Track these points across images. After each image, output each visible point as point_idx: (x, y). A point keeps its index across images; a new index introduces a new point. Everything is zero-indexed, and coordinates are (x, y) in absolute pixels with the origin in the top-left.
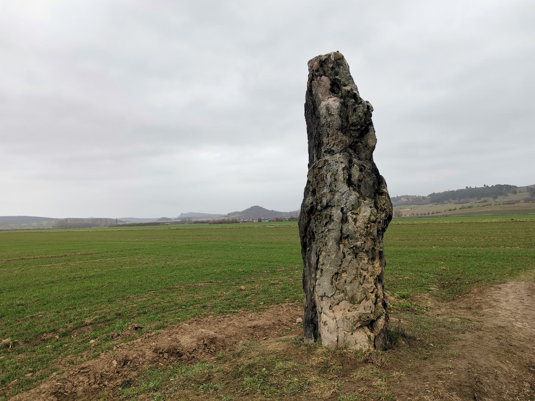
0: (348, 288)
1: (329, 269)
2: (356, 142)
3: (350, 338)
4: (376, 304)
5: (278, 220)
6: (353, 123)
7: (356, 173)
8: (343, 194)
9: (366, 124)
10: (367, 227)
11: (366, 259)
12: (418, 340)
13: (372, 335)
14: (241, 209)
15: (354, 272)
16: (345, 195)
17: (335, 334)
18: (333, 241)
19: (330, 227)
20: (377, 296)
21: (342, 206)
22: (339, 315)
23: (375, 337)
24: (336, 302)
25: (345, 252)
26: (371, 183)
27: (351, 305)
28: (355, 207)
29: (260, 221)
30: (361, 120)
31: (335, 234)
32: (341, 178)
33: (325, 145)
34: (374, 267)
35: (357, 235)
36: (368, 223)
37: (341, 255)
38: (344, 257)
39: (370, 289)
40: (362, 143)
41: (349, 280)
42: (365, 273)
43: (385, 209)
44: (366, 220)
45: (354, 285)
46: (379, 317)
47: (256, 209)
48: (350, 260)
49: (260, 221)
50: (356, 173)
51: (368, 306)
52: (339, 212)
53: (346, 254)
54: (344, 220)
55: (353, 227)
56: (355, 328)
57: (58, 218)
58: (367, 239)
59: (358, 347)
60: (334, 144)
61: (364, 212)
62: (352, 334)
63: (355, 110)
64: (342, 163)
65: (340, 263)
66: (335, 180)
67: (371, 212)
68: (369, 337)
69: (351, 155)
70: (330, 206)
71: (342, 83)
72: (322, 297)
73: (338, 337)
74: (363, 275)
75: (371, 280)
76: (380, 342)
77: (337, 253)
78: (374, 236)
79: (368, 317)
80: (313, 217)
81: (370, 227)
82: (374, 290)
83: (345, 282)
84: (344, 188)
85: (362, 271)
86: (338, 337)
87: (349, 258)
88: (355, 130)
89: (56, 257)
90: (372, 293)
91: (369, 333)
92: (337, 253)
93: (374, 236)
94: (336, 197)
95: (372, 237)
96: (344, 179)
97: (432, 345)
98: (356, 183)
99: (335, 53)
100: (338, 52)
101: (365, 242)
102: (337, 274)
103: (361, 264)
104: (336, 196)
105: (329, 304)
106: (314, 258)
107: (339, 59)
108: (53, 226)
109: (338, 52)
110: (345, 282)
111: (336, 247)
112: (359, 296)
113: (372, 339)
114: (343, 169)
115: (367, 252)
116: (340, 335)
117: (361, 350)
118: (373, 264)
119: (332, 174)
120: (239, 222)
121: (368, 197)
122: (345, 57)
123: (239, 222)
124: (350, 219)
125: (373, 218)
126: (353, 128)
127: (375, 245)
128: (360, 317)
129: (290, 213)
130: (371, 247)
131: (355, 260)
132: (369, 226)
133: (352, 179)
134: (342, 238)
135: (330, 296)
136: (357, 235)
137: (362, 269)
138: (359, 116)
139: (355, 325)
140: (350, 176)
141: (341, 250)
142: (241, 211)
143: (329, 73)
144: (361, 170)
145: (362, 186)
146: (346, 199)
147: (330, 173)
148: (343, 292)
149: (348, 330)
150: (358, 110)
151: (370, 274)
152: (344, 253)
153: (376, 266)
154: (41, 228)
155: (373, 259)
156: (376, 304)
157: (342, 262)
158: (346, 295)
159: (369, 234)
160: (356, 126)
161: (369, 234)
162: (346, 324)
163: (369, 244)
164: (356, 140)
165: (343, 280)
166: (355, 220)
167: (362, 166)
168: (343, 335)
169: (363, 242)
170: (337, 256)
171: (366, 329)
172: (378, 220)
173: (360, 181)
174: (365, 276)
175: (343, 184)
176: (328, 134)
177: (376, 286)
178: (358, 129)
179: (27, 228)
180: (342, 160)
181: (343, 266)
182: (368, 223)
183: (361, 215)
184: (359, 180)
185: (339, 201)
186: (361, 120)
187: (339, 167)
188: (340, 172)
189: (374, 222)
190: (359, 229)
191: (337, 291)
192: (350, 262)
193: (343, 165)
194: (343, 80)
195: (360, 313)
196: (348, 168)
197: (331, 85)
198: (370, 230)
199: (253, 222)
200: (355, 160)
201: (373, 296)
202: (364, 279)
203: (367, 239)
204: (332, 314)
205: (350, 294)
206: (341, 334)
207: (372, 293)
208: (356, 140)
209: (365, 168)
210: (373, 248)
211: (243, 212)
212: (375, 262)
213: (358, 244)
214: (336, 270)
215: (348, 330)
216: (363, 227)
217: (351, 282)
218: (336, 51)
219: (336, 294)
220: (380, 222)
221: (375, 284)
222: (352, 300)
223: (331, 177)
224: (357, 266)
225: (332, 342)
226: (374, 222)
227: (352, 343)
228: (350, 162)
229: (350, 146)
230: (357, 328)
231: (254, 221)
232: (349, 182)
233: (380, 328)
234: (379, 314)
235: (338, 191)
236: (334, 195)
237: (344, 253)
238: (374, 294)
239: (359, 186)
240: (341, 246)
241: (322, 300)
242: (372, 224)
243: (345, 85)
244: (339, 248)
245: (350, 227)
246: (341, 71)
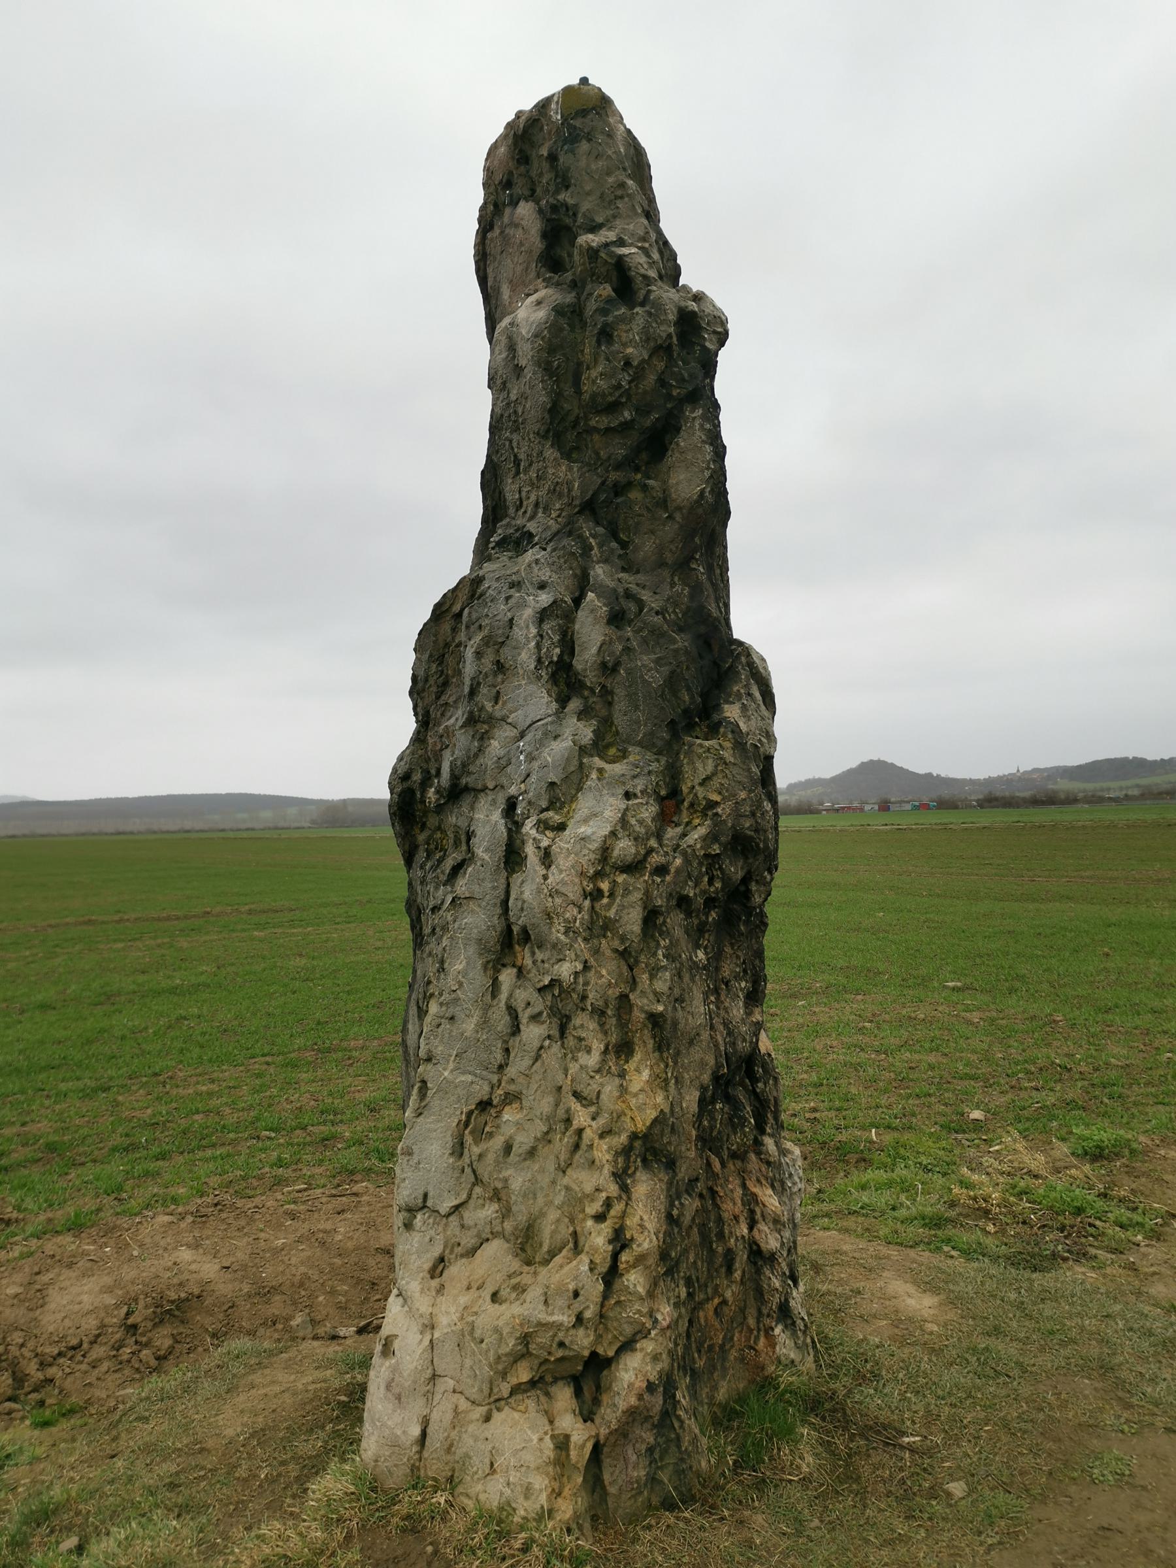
0: (518, 1182)
1: (454, 1081)
2: (619, 490)
3: (476, 1441)
4: (611, 1275)
5: (945, 805)
6: (594, 396)
7: (591, 632)
8: (522, 735)
9: (669, 397)
10: (596, 895)
11: (597, 1046)
12: (912, 1449)
13: (580, 1435)
14: (829, 771)
15: (545, 1105)
16: (528, 738)
17: (417, 1407)
18: (472, 950)
19: (462, 885)
20: (620, 1241)
21: (513, 790)
22: (448, 1315)
23: (597, 1449)
24: (468, 1240)
25: (519, 1005)
26: (656, 678)
27: (516, 1265)
28: (560, 796)
29: (885, 806)
30: (636, 378)
31: (477, 921)
32: (526, 658)
33: (511, 511)
34: (623, 1090)
35: (557, 933)
36: (599, 875)
37: (501, 1021)
38: (516, 1030)
39: (591, 1198)
40: (645, 488)
41: (523, 1141)
42: (581, 1117)
43: (713, 805)
44: (588, 858)
45: (542, 1170)
46: (627, 1346)
47: (875, 770)
48: (536, 1044)
49: (885, 806)
50: (591, 632)
51: (560, 1291)
52: (497, 816)
53: (524, 1018)
54: (512, 857)
55: (539, 891)
56: (505, 1389)
57: (325, 797)
58: (596, 952)
59: (492, 1493)
60: (537, 505)
61: (586, 821)
62: (487, 1418)
63: (606, 335)
64: (542, 586)
65: (499, 1056)
66: (500, 667)
67: (623, 821)
68: (562, 1444)
69: (587, 549)
70: (467, 789)
71: (580, 220)
72: (411, 1210)
73: (425, 1423)
74: (576, 1124)
75: (603, 1152)
76: (627, 1472)
77: (487, 1008)
78: (623, 939)
79: (561, 1344)
80: (421, 838)
81: (612, 895)
82: (608, 1204)
83: (508, 1148)
84: (531, 700)
85: (575, 1105)
86: (425, 1423)
87: (532, 1033)
88: (608, 430)
89: (178, 918)
90: (600, 1218)
91: (568, 1423)
92: (487, 1008)
93: (623, 939)
94: (495, 747)
95: (616, 944)
96: (539, 661)
97: (957, 1488)
98: (591, 679)
99: (568, 91)
100: (584, 81)
101: (586, 967)
102: (484, 1105)
103: (573, 1068)
104: (495, 743)
105: (436, 1251)
106: (414, 1024)
107: (583, 113)
108: (313, 822)
109: (584, 81)
110: (508, 1148)
111: (478, 979)
112: (550, 1229)
113: (579, 1454)
114: (543, 615)
115: (599, 1013)
116: (435, 1416)
117: (507, 1508)
118: (622, 1075)
119: (487, 641)
120: (818, 812)
121: (640, 744)
122: (620, 104)
123: (818, 812)
124: (530, 849)
125: (624, 848)
126: (601, 421)
127: (634, 983)
128: (525, 1339)
129: (990, 781)
130: (613, 993)
131: (556, 1048)
132: (605, 886)
133: (578, 664)
134: (509, 942)
135: (445, 1207)
136: (557, 933)
137: (576, 1094)
138: (628, 364)
139: (504, 1375)
140: (568, 644)
141: (503, 996)
142: (827, 775)
143: (564, 194)
144: (616, 619)
145: (620, 692)
146: (531, 758)
147: (478, 638)
148: (496, 1196)
149: (473, 1392)
150: (621, 334)
151: (602, 1121)
152: (512, 1011)
153: (635, 1087)
154: (281, 824)
155: (624, 1049)
156: (611, 1275)
157: (507, 1050)
158: (506, 1213)
159: (605, 928)
160: (612, 408)
161: (605, 928)
162: (468, 1362)
163: (605, 977)
164: (614, 476)
165: (498, 1142)
166: (547, 858)
167: (628, 595)
168: (449, 1415)
169: (579, 967)
170: (484, 1023)
171: (564, 1396)
172: (656, 859)
173: (608, 669)
174: (580, 1131)
175: (532, 688)
176: (517, 463)
177: (625, 1188)
178: (626, 426)
179: (250, 825)
180: (545, 574)
181: (511, 1071)
182: (599, 875)
183: (577, 829)
184: (604, 665)
185: (503, 765)
186: (636, 378)
187: (523, 605)
188: (526, 631)
189: (632, 867)
190: (558, 901)
191: (478, 1190)
192: (537, 1058)
193: (545, 599)
194: (585, 206)
195: (525, 1321)
196: (560, 616)
197: (544, 235)
198: (609, 906)
199: (862, 810)
200: (599, 572)
201: (599, 1238)
202: (577, 1147)
203: (596, 952)
204: (423, 1304)
205: (521, 1214)
206: (441, 1415)
207: (600, 1218)
208: (614, 476)
209: (641, 604)
210: (624, 997)
211: (834, 779)
212: (631, 1066)
213: (565, 970)
214: (481, 1090)
215: (473, 1392)
216: (574, 892)
217: (532, 1153)
218: (575, 81)
219: (472, 1202)
220: (661, 870)
221: (621, 1177)
222: (526, 1245)
223: (479, 654)
224: (560, 1077)
225: (395, 1444)
226: (632, 867)
227: (479, 1464)
228: (583, 584)
229: (589, 507)
230: (514, 1391)
231: (867, 808)
232: (563, 678)
233: (622, 1405)
234: (628, 1330)
235: (504, 719)
236: (484, 737)
237: (512, 1011)
238: (606, 1228)
239: (607, 693)
240: (507, 977)
241: (408, 1226)
242: (621, 878)
243: (594, 229)
244: (495, 986)
245: (529, 888)
246: (583, 163)
